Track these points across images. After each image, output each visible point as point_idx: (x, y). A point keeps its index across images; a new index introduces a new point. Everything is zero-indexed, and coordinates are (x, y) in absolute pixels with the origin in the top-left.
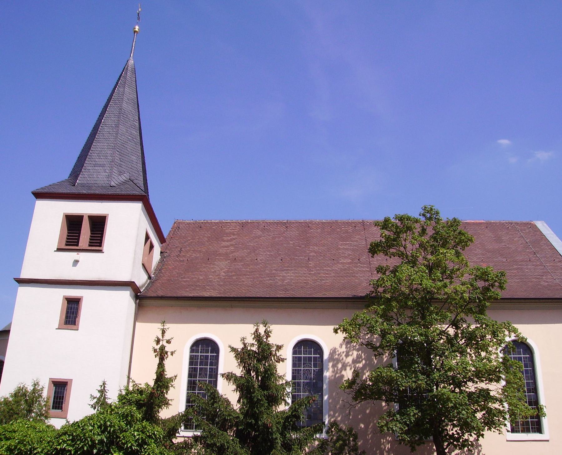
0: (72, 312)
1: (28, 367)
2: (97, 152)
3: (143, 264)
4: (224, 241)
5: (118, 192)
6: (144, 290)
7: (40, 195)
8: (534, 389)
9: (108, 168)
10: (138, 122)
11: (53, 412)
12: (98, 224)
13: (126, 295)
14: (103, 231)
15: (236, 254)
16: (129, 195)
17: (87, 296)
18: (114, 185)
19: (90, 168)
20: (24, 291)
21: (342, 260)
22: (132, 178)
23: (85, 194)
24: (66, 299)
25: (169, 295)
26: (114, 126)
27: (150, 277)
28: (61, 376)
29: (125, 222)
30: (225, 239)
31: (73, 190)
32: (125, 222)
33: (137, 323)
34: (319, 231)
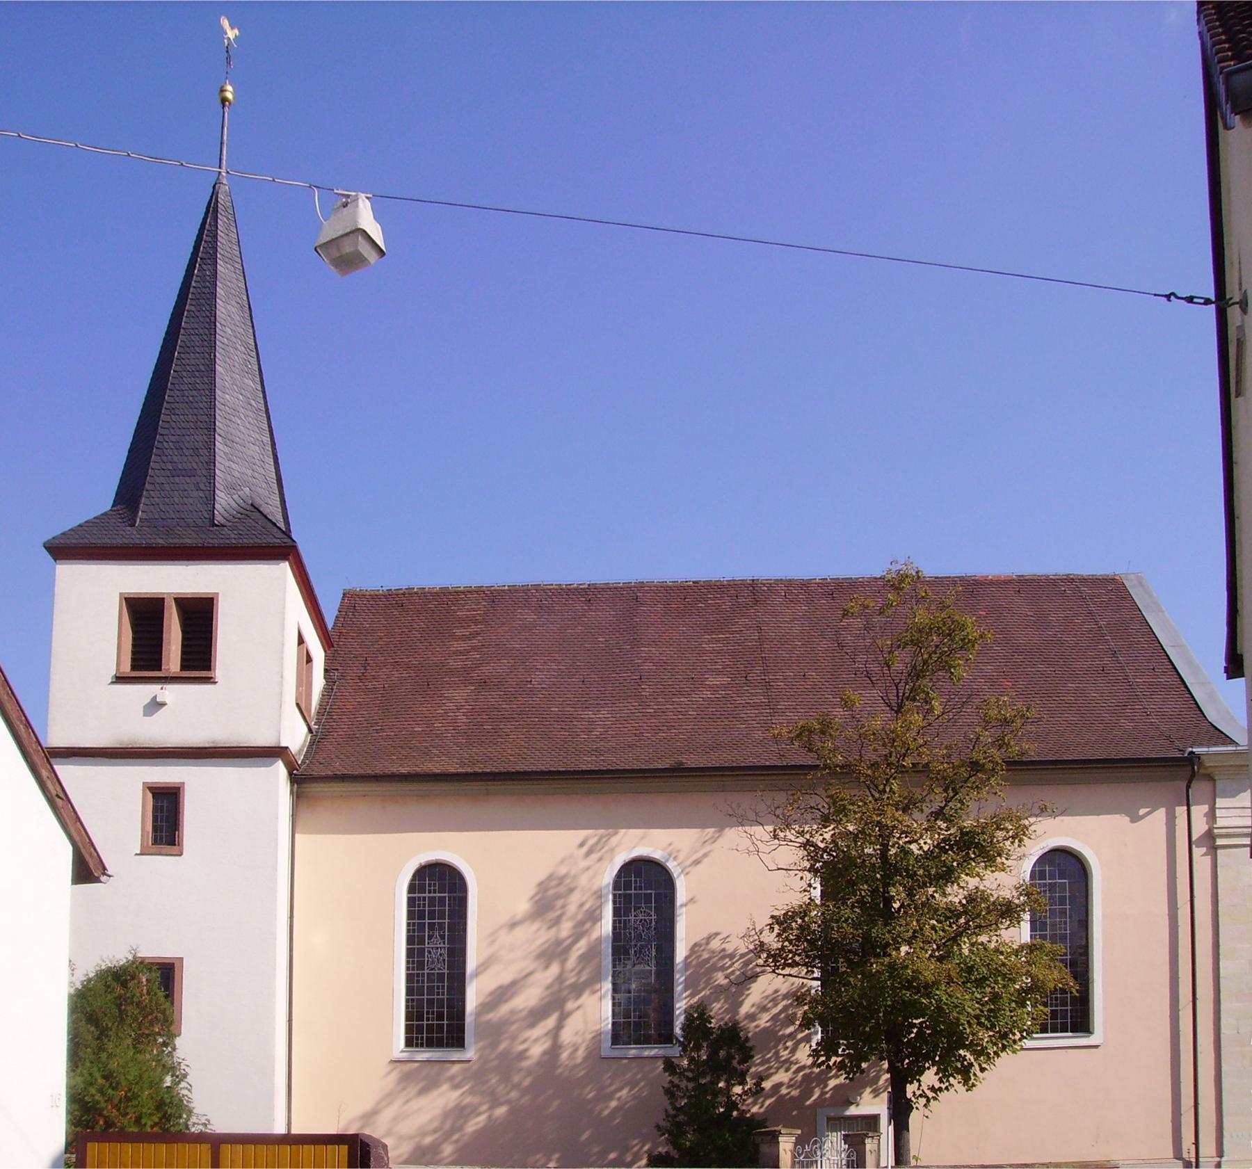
0: (165, 819)
1: (1244, 799)
2: (173, 439)
5: (233, 539)
9: (204, 479)
12: (199, 614)
14: (211, 632)
15: (486, 670)
17: (195, 781)
18: (223, 521)
19: (162, 480)
22: (258, 501)
24: (150, 788)
26: (202, 368)
29: (263, 611)
30: (458, 632)
31: (132, 536)
32: (263, 611)
33: (297, 836)
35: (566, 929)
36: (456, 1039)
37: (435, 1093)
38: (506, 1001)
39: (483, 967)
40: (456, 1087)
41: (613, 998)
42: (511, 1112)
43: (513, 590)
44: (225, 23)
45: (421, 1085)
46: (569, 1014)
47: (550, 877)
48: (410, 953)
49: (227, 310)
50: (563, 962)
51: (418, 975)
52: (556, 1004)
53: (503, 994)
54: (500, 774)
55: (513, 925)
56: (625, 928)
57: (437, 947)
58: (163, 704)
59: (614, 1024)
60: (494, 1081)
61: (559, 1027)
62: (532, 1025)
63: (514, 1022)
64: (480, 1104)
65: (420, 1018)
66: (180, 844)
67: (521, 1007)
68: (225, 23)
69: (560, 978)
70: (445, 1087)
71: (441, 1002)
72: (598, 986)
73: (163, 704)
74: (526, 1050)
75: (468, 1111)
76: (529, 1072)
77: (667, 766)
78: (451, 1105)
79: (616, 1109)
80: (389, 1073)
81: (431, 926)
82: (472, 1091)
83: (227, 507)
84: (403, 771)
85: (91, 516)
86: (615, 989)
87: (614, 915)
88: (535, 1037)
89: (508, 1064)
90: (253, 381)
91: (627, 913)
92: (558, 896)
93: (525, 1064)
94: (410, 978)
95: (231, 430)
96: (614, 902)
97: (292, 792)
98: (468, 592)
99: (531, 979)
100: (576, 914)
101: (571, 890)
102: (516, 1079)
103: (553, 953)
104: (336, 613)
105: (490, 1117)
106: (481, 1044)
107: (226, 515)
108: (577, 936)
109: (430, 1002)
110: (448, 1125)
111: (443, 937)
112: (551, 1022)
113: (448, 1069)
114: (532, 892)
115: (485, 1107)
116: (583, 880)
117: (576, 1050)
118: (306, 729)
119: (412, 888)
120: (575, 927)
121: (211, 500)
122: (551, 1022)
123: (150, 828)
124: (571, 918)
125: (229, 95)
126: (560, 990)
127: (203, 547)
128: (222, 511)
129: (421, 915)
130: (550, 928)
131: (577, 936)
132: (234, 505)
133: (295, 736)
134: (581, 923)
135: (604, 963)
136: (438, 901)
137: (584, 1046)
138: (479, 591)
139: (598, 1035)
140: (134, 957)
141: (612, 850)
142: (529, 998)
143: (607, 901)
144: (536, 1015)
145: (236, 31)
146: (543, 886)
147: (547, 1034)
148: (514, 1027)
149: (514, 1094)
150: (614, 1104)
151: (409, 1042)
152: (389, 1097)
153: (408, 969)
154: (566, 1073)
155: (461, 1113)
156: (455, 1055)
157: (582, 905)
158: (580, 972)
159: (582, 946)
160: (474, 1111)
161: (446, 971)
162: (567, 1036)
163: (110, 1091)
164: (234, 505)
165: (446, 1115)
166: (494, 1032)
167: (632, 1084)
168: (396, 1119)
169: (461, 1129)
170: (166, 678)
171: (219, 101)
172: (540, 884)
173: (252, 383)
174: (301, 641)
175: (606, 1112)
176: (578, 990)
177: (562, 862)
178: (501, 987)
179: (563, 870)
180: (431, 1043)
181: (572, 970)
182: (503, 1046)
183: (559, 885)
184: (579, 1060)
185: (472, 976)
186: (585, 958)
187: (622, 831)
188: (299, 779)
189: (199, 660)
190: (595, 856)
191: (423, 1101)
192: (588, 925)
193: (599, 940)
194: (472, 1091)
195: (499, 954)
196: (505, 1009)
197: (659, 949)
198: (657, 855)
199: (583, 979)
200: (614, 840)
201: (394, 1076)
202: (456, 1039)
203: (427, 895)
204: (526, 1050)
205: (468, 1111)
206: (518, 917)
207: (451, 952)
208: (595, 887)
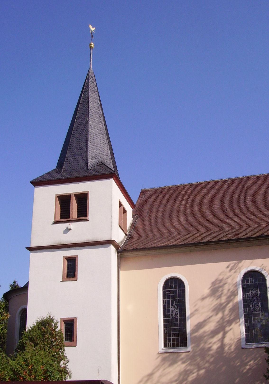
0: (71, 269)
3: (120, 226)
6: (123, 245)
7: (37, 183)
10: (102, 117)
11: (65, 342)
12: (83, 199)
13: (112, 248)
15: (191, 210)
18: (91, 168)
19: (71, 158)
20: (35, 256)
22: (104, 161)
23: (70, 178)
24: (66, 258)
25: (142, 247)
27: (126, 235)
28: (69, 315)
30: (181, 199)
31: (60, 176)
35: (224, 299)
36: (184, 344)
37: (176, 365)
38: (202, 328)
39: (192, 315)
40: (184, 363)
41: (245, 325)
42: (206, 372)
43: (201, 184)
44: (90, 26)
45: (169, 363)
46: (227, 332)
47: (216, 280)
48: (164, 312)
49: (93, 105)
50: (223, 312)
51: (168, 319)
52: (222, 328)
53: (200, 326)
54: (194, 243)
55: (203, 299)
56: (248, 297)
57: (175, 309)
58: (70, 229)
59: (246, 335)
60: (199, 360)
61: (223, 337)
62: (212, 337)
63: (206, 336)
64: (194, 369)
65: (169, 336)
66: (76, 277)
67: (208, 330)
68: (90, 26)
69: (223, 318)
70: (180, 363)
71: (177, 330)
72: (238, 321)
73: (70, 229)
74: (211, 347)
75: (189, 372)
76: (212, 356)
77: (258, 236)
78: (182, 370)
79: (249, 369)
80: (157, 358)
81: (172, 301)
82: (190, 364)
83: (92, 164)
84: (158, 245)
85: (47, 172)
86: (246, 321)
87: (243, 293)
88: (214, 342)
89: (203, 353)
90: (102, 125)
91: (248, 291)
92: (220, 287)
93: (211, 352)
94: (165, 321)
95: (95, 141)
96: (243, 288)
97: (118, 256)
98: (185, 185)
99: (211, 319)
100: (227, 294)
101: (226, 284)
102: (208, 358)
103: (219, 308)
104: (138, 197)
105: (198, 374)
106: (193, 345)
107: (92, 166)
108: (228, 301)
109: (173, 330)
110: (181, 378)
111: (177, 305)
112: (220, 335)
113: (180, 355)
114: (210, 286)
115: (195, 370)
116: (229, 280)
117: (231, 346)
118: (124, 235)
119: (164, 288)
120: (227, 298)
121: (87, 162)
122: (220, 335)
123: (66, 272)
124: (225, 295)
125: (92, 46)
126: (223, 323)
127: (83, 177)
128: (90, 165)
129: (168, 297)
130: (217, 299)
131: (228, 301)
132: (95, 163)
133: (119, 237)
134: (229, 297)
135: (240, 311)
136: (174, 291)
137: (234, 344)
138: (189, 185)
139: (240, 340)
140: (50, 317)
141: (240, 268)
142: (210, 327)
143: (239, 288)
144: (214, 333)
145: (94, 28)
146: (214, 283)
147: (219, 340)
148: (206, 338)
149: (207, 365)
150: (248, 367)
151: (165, 346)
152: (158, 368)
153: (164, 317)
154: (227, 356)
155: (186, 373)
156: (183, 350)
157: (229, 290)
158: (231, 315)
159: (230, 305)
160: (191, 372)
161: (178, 318)
162: (227, 340)
163: (25, 366)
164: (95, 163)
165: (180, 374)
166: (198, 340)
167: (255, 359)
168: (161, 376)
169: (186, 379)
170: (71, 221)
171: (89, 48)
172: (213, 283)
173: (102, 126)
174: (120, 205)
175: (245, 371)
176: (230, 322)
177: (220, 274)
178: (199, 323)
179: (221, 277)
180: (174, 346)
181: (227, 315)
182: (202, 346)
183: (219, 283)
184: (232, 350)
185: (189, 318)
186: (233, 310)
187: (244, 261)
188: (122, 252)
189: (83, 213)
190: (233, 271)
191: (171, 369)
192: (232, 297)
193: (237, 303)
194: (190, 364)
195: (198, 310)
196: (201, 331)
197: (262, 305)
198: (258, 269)
199: (232, 318)
200: (240, 265)
201: (159, 359)
202: (184, 344)
203: (170, 290)
204: (211, 347)
205: (189, 372)
206: (205, 296)
207: (180, 311)
208: (234, 282)
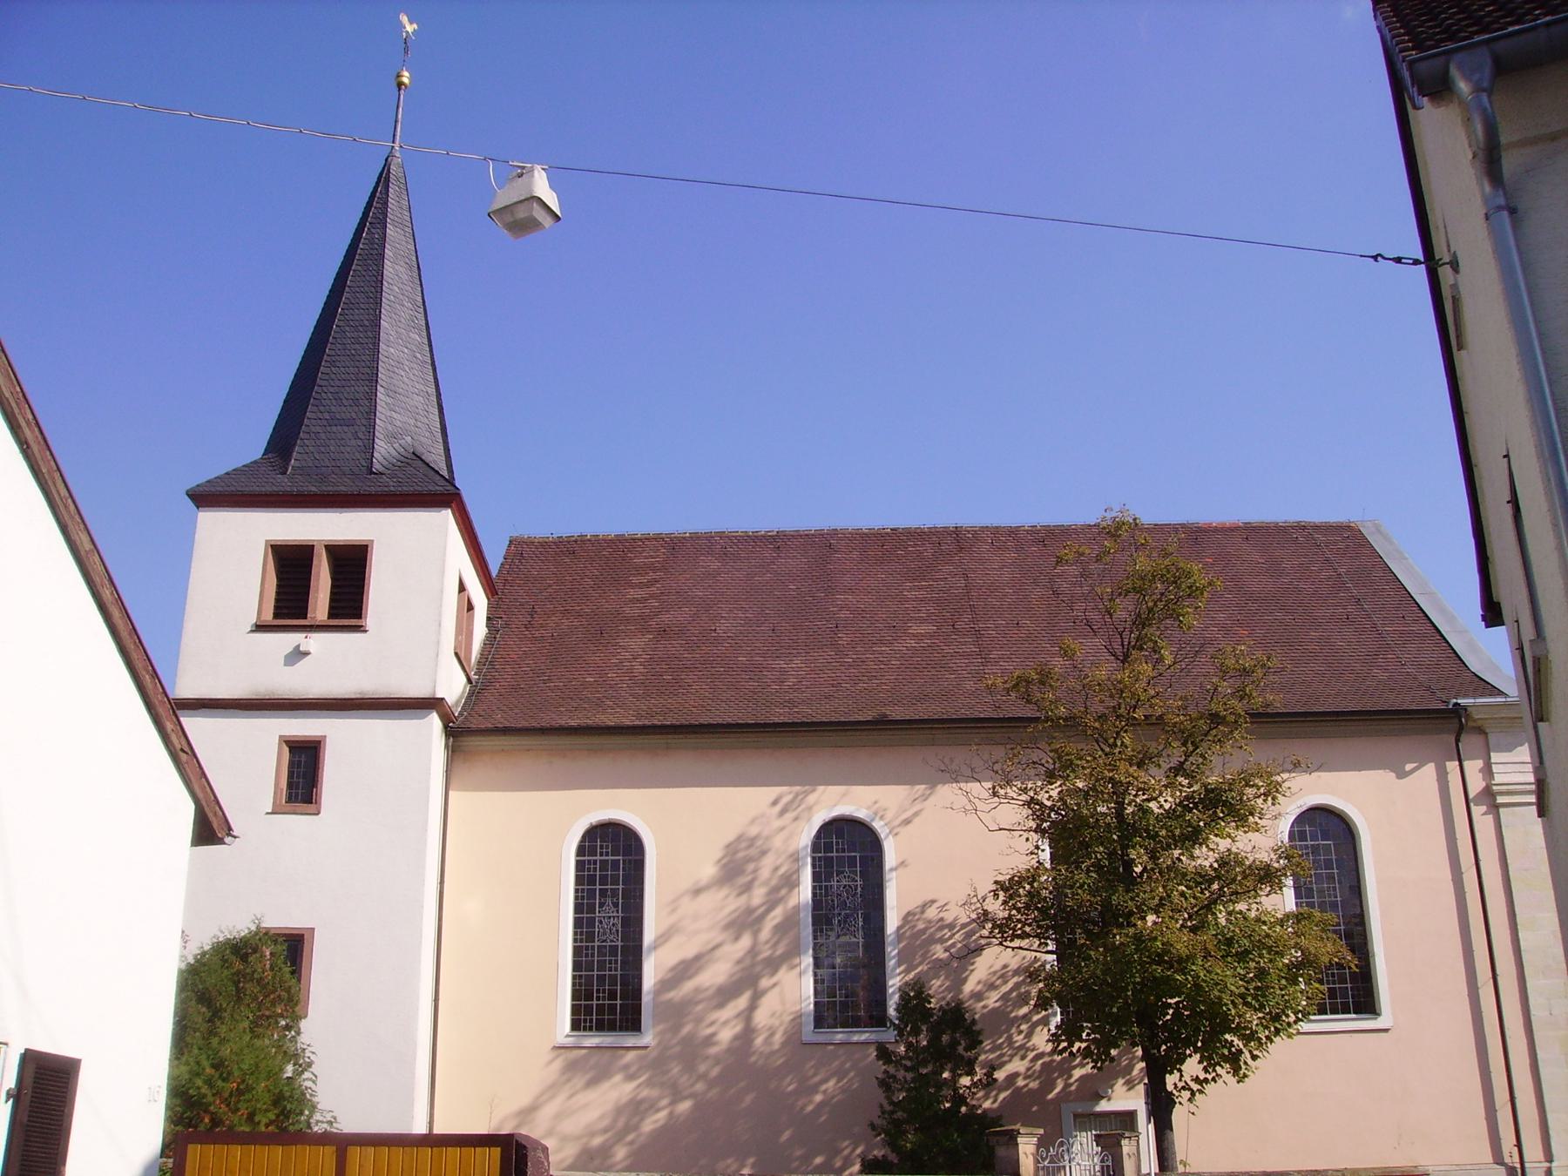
0: (303, 776)
4: (633, 586)
5: (392, 486)
7: (205, 498)
8: (1356, 889)
12: (351, 564)
15: (665, 618)
16: (421, 494)
17: (332, 730)
18: (381, 469)
19: (318, 429)
21: (915, 629)
22: (420, 450)
27: (469, 680)
30: (635, 580)
31: (283, 483)
34: (855, 554)
